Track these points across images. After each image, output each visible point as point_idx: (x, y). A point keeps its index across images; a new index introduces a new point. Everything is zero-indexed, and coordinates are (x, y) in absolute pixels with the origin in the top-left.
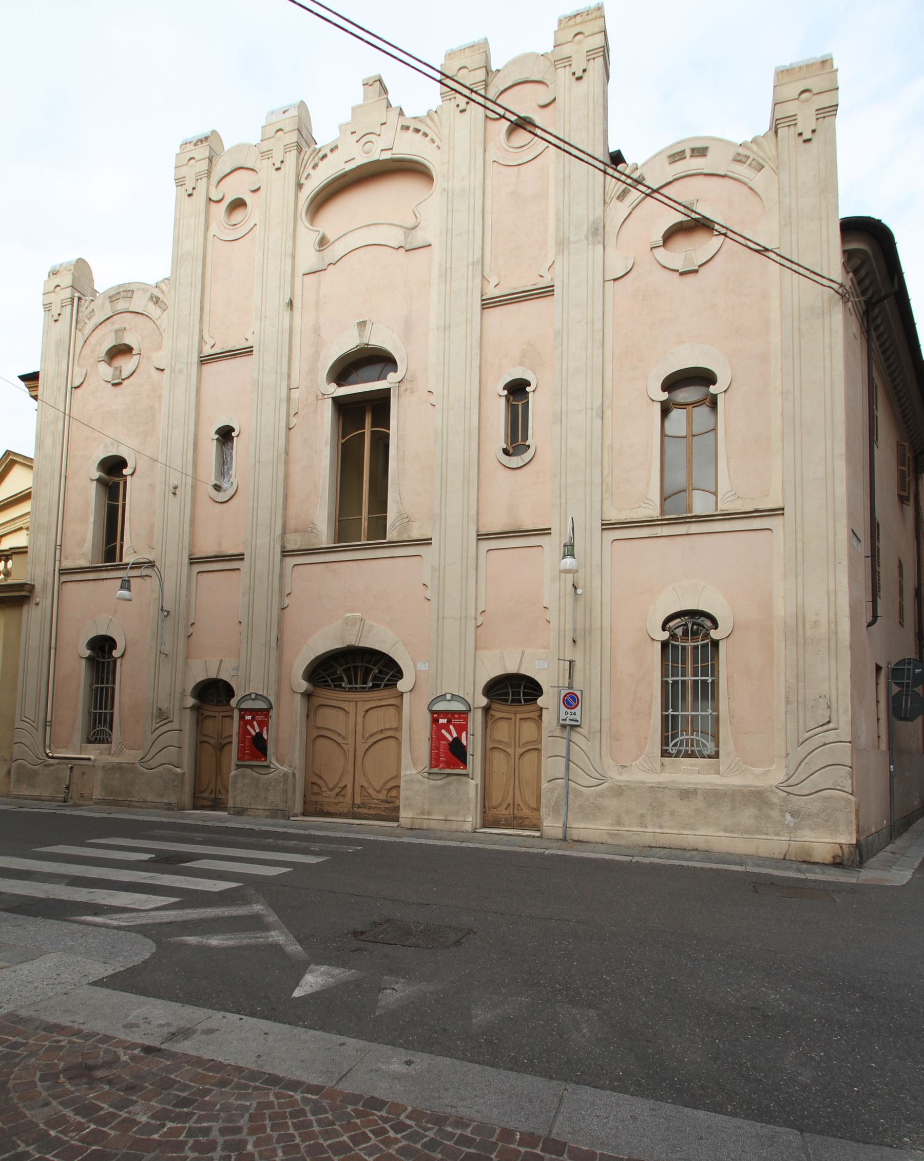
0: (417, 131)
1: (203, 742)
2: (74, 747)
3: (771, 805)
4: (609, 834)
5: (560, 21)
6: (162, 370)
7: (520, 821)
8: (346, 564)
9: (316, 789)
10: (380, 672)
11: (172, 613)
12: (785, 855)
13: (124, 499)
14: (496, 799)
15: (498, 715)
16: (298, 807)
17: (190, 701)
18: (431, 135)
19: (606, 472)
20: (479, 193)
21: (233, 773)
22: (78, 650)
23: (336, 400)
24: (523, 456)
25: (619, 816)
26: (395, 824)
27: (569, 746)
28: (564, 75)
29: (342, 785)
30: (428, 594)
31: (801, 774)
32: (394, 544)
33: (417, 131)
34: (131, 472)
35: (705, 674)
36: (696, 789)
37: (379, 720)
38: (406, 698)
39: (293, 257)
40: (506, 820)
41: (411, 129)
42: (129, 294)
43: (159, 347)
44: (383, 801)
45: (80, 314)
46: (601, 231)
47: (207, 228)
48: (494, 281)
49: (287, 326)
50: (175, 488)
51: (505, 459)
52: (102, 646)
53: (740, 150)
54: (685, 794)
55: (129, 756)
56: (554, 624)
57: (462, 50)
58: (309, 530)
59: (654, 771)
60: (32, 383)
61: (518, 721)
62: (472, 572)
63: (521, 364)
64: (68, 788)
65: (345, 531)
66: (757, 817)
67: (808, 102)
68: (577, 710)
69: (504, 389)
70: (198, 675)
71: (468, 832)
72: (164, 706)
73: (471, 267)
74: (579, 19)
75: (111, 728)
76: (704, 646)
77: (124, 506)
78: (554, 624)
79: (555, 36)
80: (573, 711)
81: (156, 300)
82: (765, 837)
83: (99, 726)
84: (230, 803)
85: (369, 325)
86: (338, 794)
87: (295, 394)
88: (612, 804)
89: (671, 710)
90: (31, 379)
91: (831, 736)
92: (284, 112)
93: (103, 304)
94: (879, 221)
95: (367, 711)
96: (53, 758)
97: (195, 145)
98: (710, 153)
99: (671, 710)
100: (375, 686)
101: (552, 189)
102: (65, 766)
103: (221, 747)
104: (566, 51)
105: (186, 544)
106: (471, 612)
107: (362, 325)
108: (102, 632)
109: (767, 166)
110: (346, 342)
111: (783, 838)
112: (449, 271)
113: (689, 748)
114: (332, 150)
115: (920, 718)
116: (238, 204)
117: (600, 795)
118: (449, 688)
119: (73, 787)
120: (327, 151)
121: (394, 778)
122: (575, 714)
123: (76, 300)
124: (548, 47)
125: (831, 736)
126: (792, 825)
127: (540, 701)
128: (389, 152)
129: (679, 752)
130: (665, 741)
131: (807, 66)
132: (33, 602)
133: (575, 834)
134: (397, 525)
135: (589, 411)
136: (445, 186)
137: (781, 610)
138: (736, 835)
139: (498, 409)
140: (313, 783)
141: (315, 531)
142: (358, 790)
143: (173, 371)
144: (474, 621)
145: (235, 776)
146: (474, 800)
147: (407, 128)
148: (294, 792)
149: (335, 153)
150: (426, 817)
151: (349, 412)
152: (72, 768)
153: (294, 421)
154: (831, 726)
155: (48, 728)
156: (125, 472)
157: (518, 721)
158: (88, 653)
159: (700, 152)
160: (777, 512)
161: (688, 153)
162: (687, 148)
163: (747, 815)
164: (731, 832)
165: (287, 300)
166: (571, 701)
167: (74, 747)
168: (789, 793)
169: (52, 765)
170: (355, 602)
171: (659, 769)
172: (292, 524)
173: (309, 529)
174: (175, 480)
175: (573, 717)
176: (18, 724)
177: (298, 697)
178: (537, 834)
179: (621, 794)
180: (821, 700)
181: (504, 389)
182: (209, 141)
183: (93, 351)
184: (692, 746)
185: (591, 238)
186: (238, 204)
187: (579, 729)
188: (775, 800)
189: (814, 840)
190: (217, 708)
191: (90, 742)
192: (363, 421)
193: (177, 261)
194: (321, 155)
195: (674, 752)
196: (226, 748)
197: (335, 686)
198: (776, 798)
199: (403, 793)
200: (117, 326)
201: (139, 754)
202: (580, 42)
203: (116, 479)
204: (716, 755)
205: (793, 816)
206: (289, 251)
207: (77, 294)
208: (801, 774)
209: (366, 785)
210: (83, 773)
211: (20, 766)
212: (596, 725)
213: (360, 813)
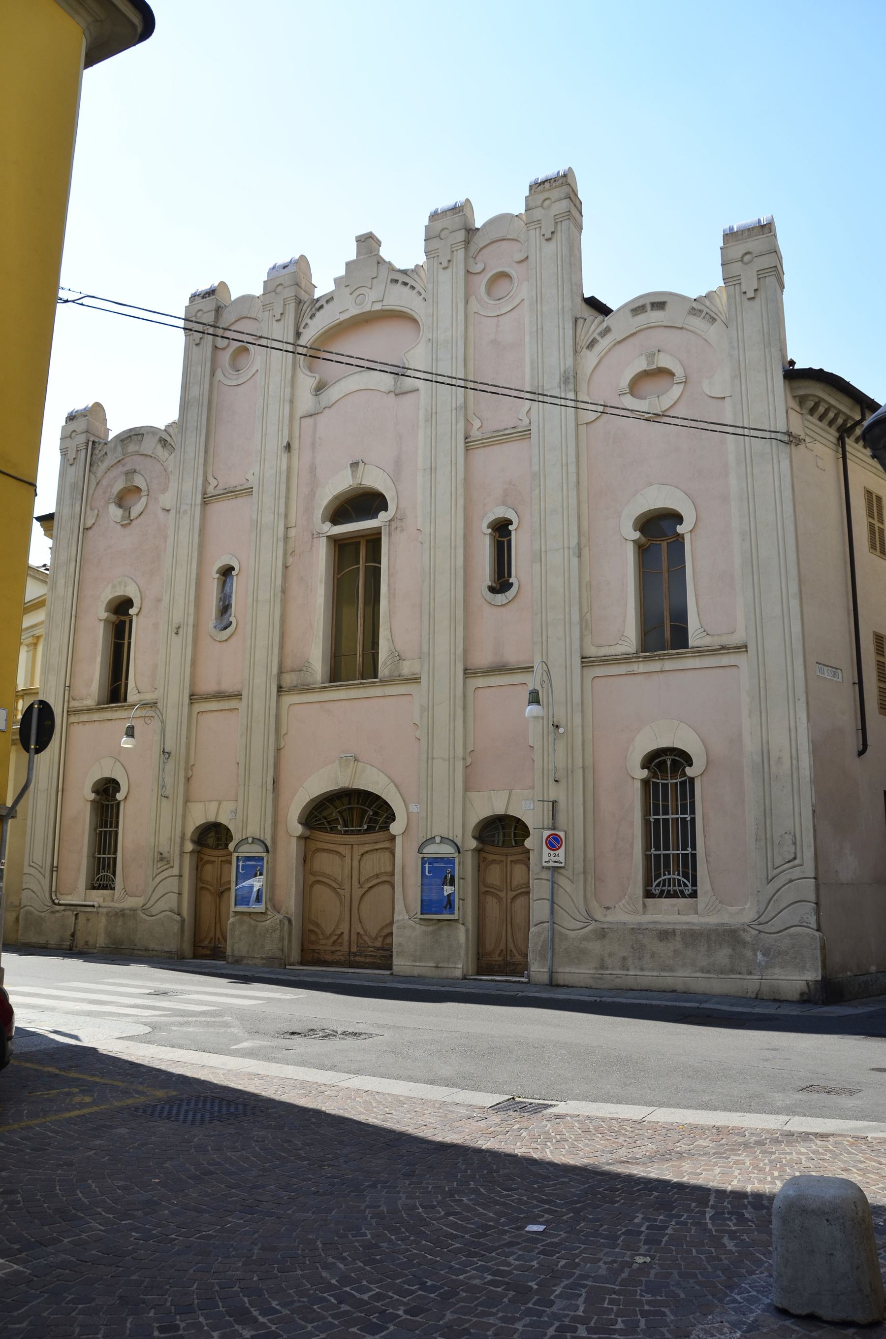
0: (405, 284)
1: (202, 888)
2: (77, 893)
3: (744, 944)
4: (593, 978)
5: (531, 187)
6: (168, 511)
7: (512, 968)
8: (339, 703)
9: (313, 938)
10: (376, 814)
11: (173, 753)
12: (757, 994)
13: (130, 638)
14: (489, 944)
15: (491, 857)
16: (295, 955)
17: (189, 847)
18: (418, 288)
19: (585, 610)
20: (461, 343)
21: (231, 920)
24: (507, 594)
25: (603, 960)
26: (388, 972)
27: (553, 888)
29: (339, 932)
30: (418, 734)
31: (771, 912)
32: (385, 682)
33: (405, 284)
34: (137, 610)
35: (684, 812)
36: (674, 931)
37: (373, 864)
38: (398, 841)
39: (291, 402)
40: (499, 966)
41: (400, 282)
42: (140, 437)
43: (165, 490)
44: (378, 949)
45: (94, 457)
46: (572, 380)
47: (213, 374)
49: (284, 467)
50: (179, 628)
51: (490, 596)
52: (107, 790)
53: (695, 305)
54: (665, 935)
55: (131, 902)
56: (538, 764)
57: (445, 212)
58: (304, 668)
59: (636, 912)
60: (48, 523)
61: (509, 864)
62: (460, 712)
63: (504, 503)
65: (337, 674)
66: (731, 957)
67: (753, 255)
68: (561, 851)
69: (488, 527)
70: (199, 816)
71: (458, 979)
72: (164, 849)
73: (454, 412)
74: (547, 185)
75: (114, 874)
76: (683, 783)
77: (129, 644)
78: (538, 764)
79: (527, 201)
81: (163, 442)
82: (739, 976)
83: (103, 873)
84: (229, 951)
85: (361, 465)
86: (335, 942)
87: (292, 533)
88: (595, 947)
89: (653, 849)
91: (796, 873)
92: (284, 268)
93: (115, 447)
95: (362, 855)
96: (59, 904)
97: (203, 297)
98: (668, 306)
99: (653, 849)
100: (370, 830)
101: (527, 339)
102: (70, 913)
103: (221, 894)
104: (538, 214)
105: (187, 684)
106: (460, 752)
107: (355, 465)
108: (107, 775)
109: (719, 320)
110: (338, 483)
111: (755, 977)
112: (434, 416)
113: (671, 888)
114: (328, 302)
117: (585, 938)
118: (440, 829)
121: (386, 926)
122: (558, 855)
123: (90, 443)
125: (796, 873)
126: (763, 963)
127: (528, 843)
128: (381, 303)
129: (662, 892)
130: (648, 883)
131: (748, 229)
133: (561, 979)
134: (389, 663)
135: (566, 550)
136: (430, 337)
137: (750, 745)
138: (712, 976)
140: (310, 930)
141: (310, 670)
142: (354, 937)
143: (178, 512)
144: (461, 761)
145: (233, 923)
146: (464, 945)
147: (396, 281)
148: (290, 941)
149: (331, 304)
150: (417, 964)
151: (343, 549)
152: (77, 915)
153: (290, 560)
154: (797, 862)
155: (55, 873)
156: (131, 611)
157: (509, 864)
158: (92, 796)
159: (659, 305)
160: (742, 648)
162: (647, 301)
163: (722, 956)
164: (708, 972)
165: (285, 444)
167: (77, 893)
168: (760, 932)
169: (58, 911)
170: (345, 740)
171: (641, 910)
172: (288, 663)
173: (302, 668)
174: (177, 617)
175: (556, 858)
176: (27, 870)
177: (294, 841)
178: (526, 980)
179: (604, 937)
180: (787, 836)
181: (488, 527)
182: (96, 411)
183: (105, 493)
184: (674, 886)
185: (562, 386)
188: (748, 939)
189: (783, 977)
190: (216, 852)
191: (94, 888)
192: (357, 564)
193: (185, 405)
194: (317, 305)
195: (657, 892)
196: (225, 895)
197: (331, 828)
198: (748, 937)
199: (396, 940)
200: (128, 467)
202: (549, 207)
203: (123, 618)
204: (694, 895)
205: (764, 955)
206: (288, 397)
208: (771, 912)
209: (362, 932)
210: (88, 920)
211: (28, 913)
212: (579, 867)
213: (359, 962)
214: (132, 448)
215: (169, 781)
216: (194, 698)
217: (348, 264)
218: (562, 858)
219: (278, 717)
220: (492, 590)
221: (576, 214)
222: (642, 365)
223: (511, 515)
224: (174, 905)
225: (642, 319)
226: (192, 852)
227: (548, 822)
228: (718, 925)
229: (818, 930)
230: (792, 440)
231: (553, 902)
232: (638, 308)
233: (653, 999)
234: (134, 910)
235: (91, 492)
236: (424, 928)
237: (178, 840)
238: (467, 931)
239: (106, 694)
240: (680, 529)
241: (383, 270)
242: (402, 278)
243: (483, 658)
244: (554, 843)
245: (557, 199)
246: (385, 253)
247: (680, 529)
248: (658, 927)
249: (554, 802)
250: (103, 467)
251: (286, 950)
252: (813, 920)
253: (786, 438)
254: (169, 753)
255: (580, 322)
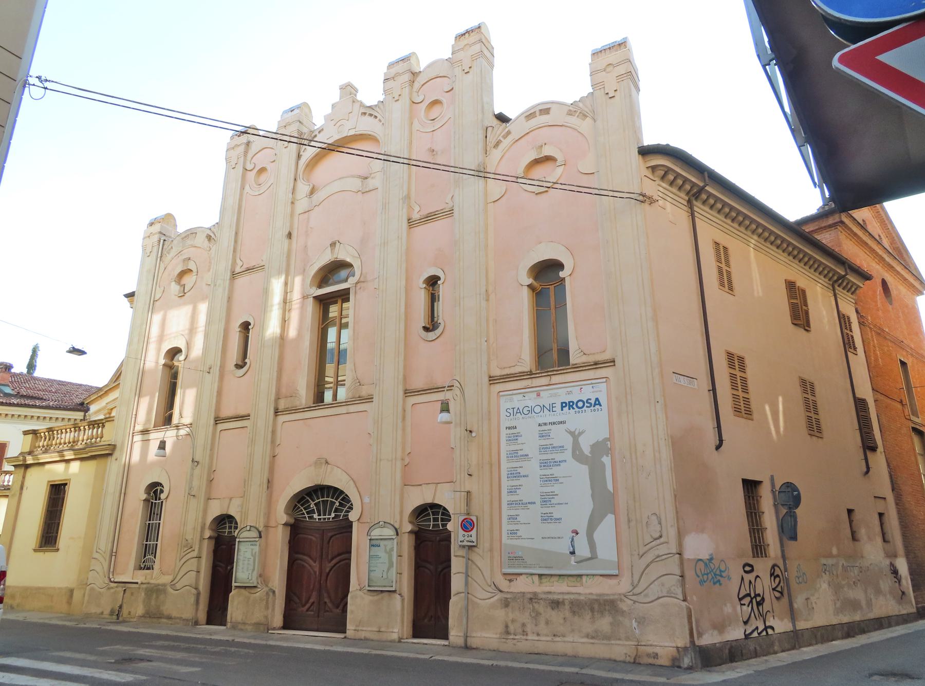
3: (623, 613)
18: (379, 117)
22: (138, 494)
23: (316, 298)
26: (342, 636)
28: (458, 71)
33: (371, 115)
47: (243, 188)
48: (417, 209)
51: (424, 333)
62: (400, 424)
64: (121, 607)
67: (615, 67)
68: (474, 533)
80: (470, 533)
90: (130, 296)
91: (662, 550)
94: (668, 145)
98: (551, 112)
104: (460, 55)
115: (878, 57)
116: (262, 170)
119: (125, 606)
120: (317, 133)
124: (448, 55)
132: (114, 457)
133: (473, 642)
139: (421, 297)
147: (365, 114)
149: (322, 133)
154: (662, 540)
159: (545, 111)
161: (538, 113)
162: (537, 109)
163: (604, 623)
164: (593, 638)
166: (467, 525)
168: (635, 602)
172: (284, 391)
175: (470, 539)
182: (169, 218)
186: (262, 170)
187: (475, 549)
188: (625, 608)
191: (141, 568)
201: (170, 578)
207: (163, 238)
210: (132, 594)
212: (487, 545)
214: (189, 242)
215: (195, 483)
216: (218, 420)
217: (333, 106)
218: (474, 538)
219: (274, 432)
220: (426, 329)
221: (488, 55)
222: (533, 156)
223: (440, 273)
224: (193, 582)
225: (534, 122)
226: (210, 538)
227: (463, 509)
228: (600, 595)
229: (684, 600)
230: (645, 199)
231: (467, 576)
232: (530, 115)
233: (546, 664)
234: (164, 585)
235: (160, 275)
236: (371, 598)
237: (199, 530)
238: (403, 600)
239: (161, 419)
240: (562, 274)
241: (357, 106)
242: (369, 111)
243: (418, 382)
244: (467, 525)
245: (474, 42)
246: (359, 97)
247: (562, 274)
248: (551, 597)
249: (468, 492)
250: (169, 257)
251: (269, 616)
252: (679, 591)
253: (641, 198)
254: (198, 462)
255: (490, 129)
